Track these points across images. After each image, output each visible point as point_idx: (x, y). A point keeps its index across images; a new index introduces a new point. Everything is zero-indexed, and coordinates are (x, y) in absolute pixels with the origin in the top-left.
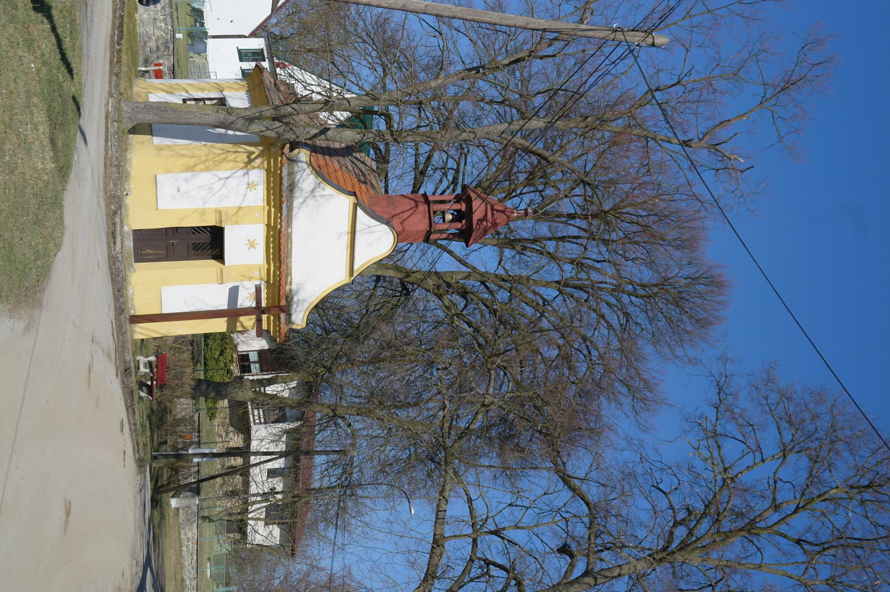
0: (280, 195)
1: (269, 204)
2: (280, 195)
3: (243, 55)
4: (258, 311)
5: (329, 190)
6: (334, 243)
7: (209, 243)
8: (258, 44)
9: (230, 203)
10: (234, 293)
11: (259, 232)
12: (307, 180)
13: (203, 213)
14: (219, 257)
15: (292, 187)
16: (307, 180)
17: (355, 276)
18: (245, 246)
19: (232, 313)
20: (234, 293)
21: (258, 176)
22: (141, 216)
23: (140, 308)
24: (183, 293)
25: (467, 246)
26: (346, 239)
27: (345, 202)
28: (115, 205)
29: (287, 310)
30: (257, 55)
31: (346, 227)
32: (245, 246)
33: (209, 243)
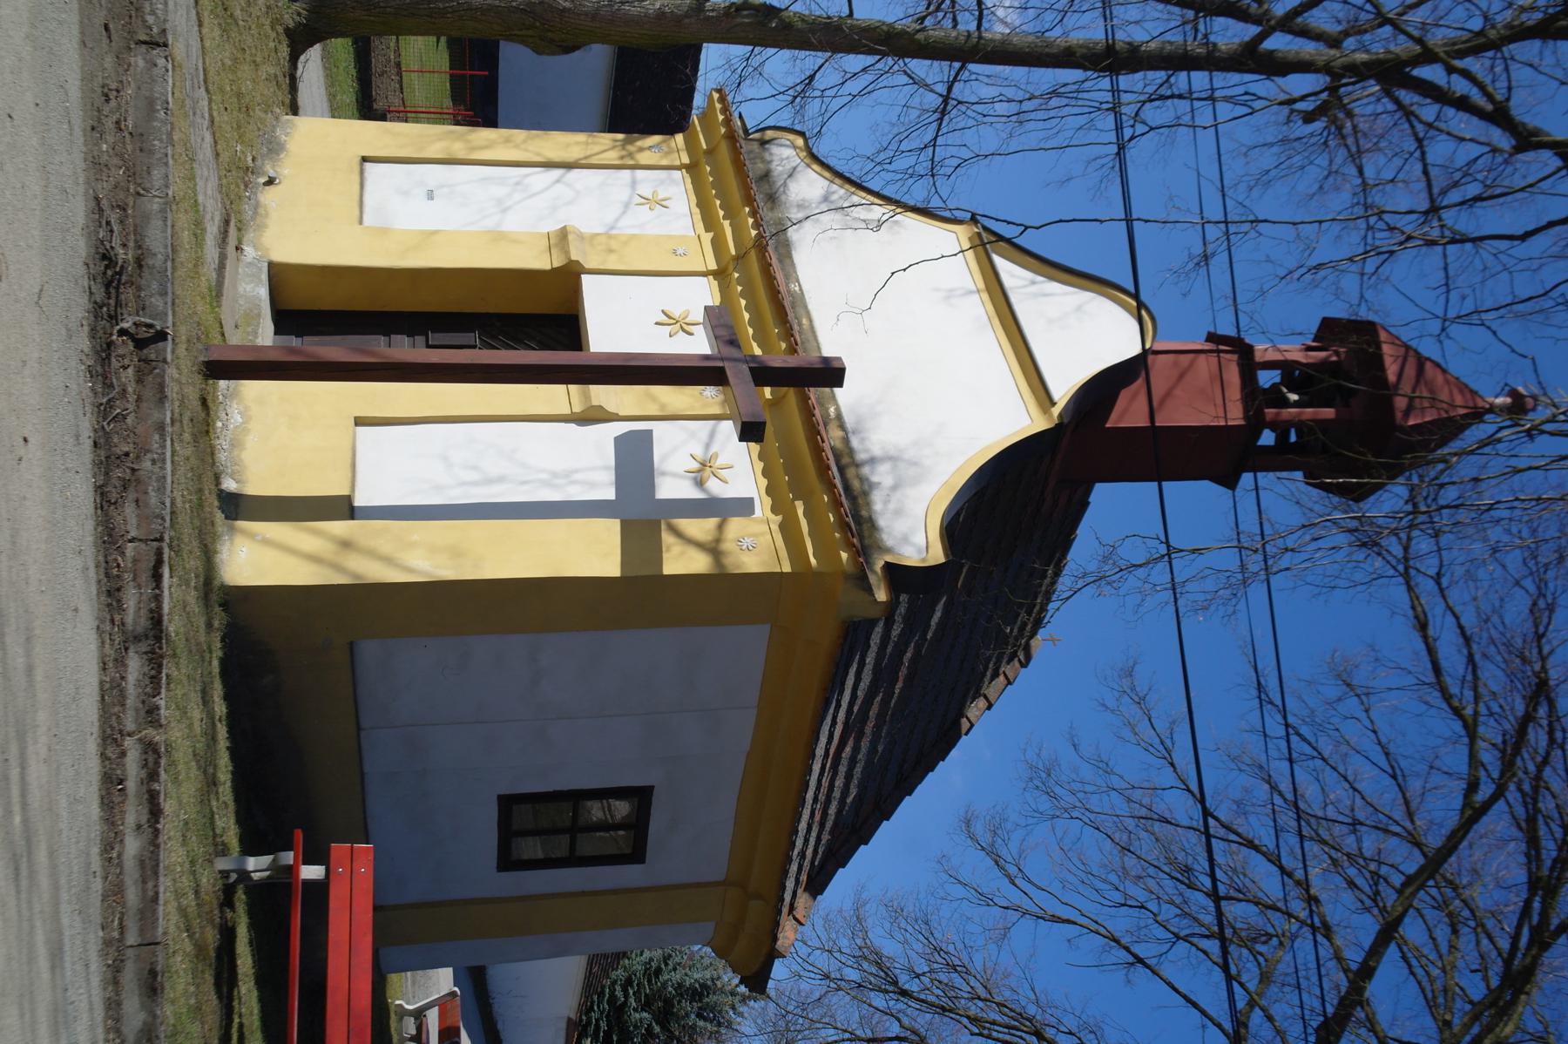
1: (710, 223)
13: (498, 237)
16: (808, 186)
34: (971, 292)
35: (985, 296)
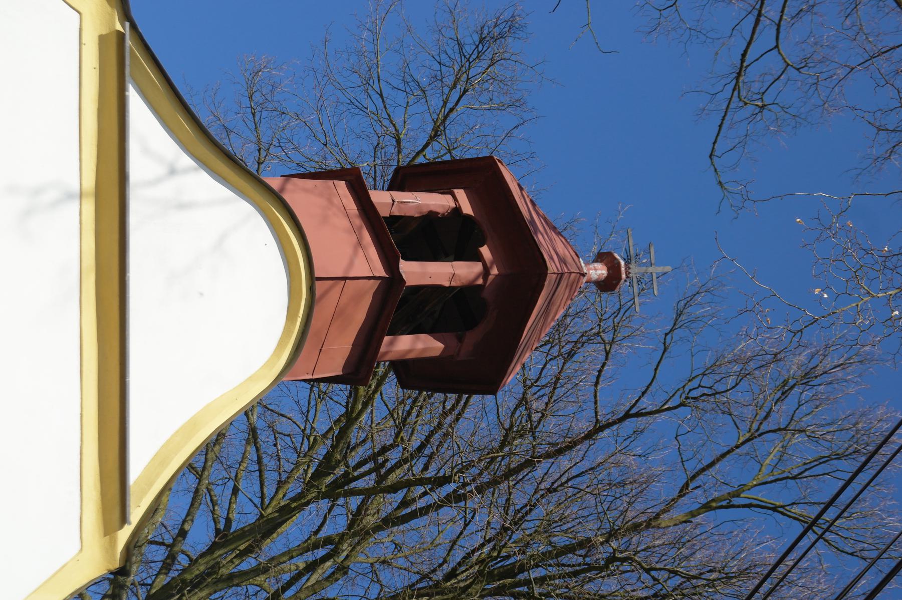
17: (136, 514)
26: (67, 239)
31: (65, 157)
34: (69, 196)
35: (89, 207)
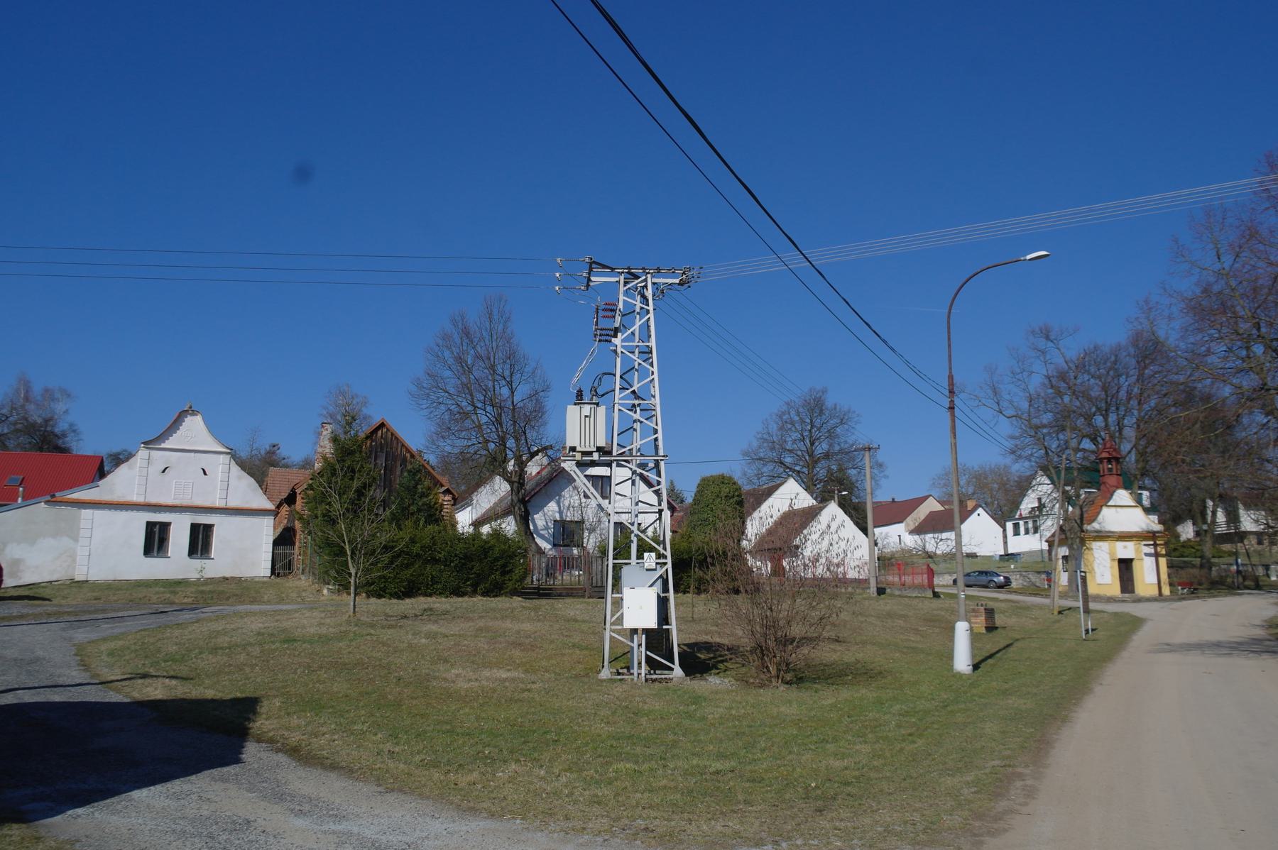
0: (1103, 536)
2: (1103, 536)
3: (1017, 533)
4: (1155, 545)
5: (1100, 517)
6: (1124, 513)
7: (1125, 566)
8: (1009, 525)
9: (1107, 557)
10: (1146, 555)
11: (1120, 545)
12: (1095, 525)
14: (1131, 560)
15: (1097, 531)
16: (1095, 525)
18: (1126, 550)
19: (1157, 555)
20: (1146, 555)
21: (1096, 545)
22: (1116, 590)
23: (1155, 592)
24: (1148, 574)
25: (816, 406)
27: (1105, 511)
28: (1111, 600)
29: (1154, 533)
30: (1016, 526)
32: (1126, 550)
33: (1125, 566)
